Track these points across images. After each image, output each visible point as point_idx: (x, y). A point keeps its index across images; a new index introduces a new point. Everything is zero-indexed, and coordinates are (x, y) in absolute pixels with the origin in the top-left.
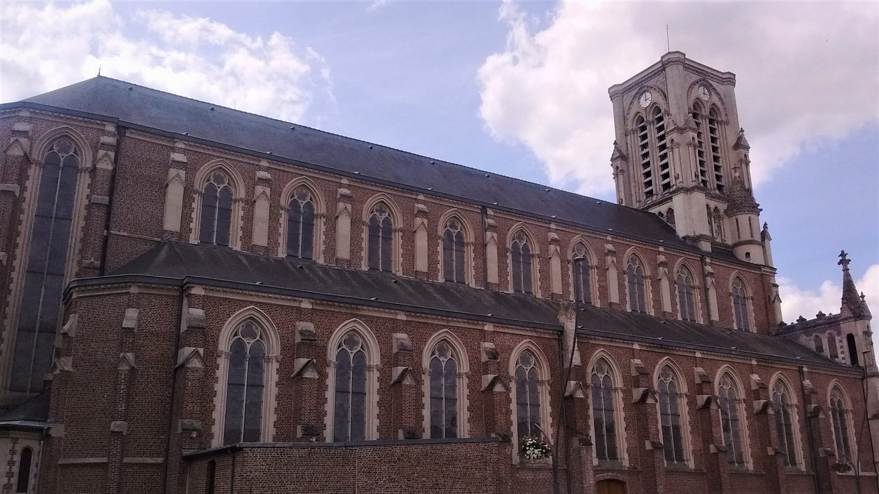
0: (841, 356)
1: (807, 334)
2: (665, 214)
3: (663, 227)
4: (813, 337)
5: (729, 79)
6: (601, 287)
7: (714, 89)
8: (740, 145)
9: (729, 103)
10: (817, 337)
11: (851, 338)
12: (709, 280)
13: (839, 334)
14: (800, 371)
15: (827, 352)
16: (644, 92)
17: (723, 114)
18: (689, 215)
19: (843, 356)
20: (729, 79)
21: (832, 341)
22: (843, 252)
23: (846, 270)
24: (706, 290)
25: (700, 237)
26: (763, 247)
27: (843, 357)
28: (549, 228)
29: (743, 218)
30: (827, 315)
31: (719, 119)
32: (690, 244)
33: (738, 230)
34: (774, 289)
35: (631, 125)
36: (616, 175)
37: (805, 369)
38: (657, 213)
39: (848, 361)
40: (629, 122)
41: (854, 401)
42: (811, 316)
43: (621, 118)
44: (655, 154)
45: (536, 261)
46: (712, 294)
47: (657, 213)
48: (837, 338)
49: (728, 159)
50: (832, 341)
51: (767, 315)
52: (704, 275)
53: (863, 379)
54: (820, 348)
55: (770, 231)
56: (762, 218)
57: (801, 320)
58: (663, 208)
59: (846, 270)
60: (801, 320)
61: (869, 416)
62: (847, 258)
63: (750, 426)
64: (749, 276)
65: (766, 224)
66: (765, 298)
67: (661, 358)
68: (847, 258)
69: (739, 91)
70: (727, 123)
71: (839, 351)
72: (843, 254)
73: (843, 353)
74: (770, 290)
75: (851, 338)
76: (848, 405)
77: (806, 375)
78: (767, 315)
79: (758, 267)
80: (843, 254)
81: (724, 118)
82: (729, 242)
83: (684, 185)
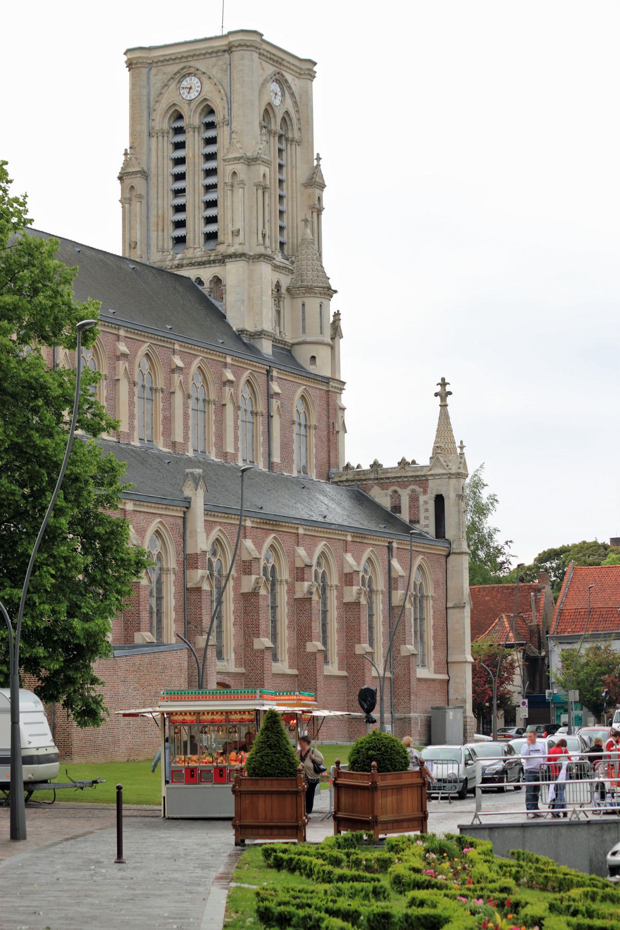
0: (423, 522)
1: (383, 487)
2: (207, 284)
3: (205, 304)
4: (390, 492)
5: (307, 69)
6: (165, 418)
7: (289, 87)
8: (315, 182)
9: (303, 105)
10: (395, 492)
11: (439, 500)
12: (275, 403)
13: (425, 492)
14: (390, 548)
15: (405, 516)
16: (189, 74)
17: (296, 127)
18: (248, 299)
19: (427, 522)
20: (307, 69)
21: (414, 499)
22: (443, 379)
23: (444, 406)
24: (270, 417)
25: (260, 334)
26: (332, 348)
27: (427, 524)
28: (118, 336)
29: (312, 303)
30: (380, 430)
31: (290, 135)
32: (245, 342)
33: (304, 320)
34: (340, 414)
35: (162, 123)
36: (126, 201)
37: (395, 545)
38: (193, 279)
39: (432, 530)
40: (157, 116)
41: (437, 584)
42: (390, 462)
43: (141, 105)
44: (195, 182)
45: (103, 383)
46: (276, 423)
47: (193, 279)
48: (422, 499)
49: (296, 209)
50: (414, 499)
51: (329, 452)
52: (270, 396)
53: (448, 556)
54: (397, 508)
55: (344, 325)
56: (335, 305)
57: (376, 465)
58: (206, 274)
59: (444, 406)
60: (376, 465)
61: (449, 605)
62: (448, 388)
63: (340, 617)
64: (316, 392)
65: (337, 314)
66: (329, 426)
67: (267, 536)
68: (448, 388)
69: (318, 87)
70: (299, 143)
71: (422, 515)
72: (443, 384)
73: (427, 518)
74: (336, 415)
75: (439, 500)
76: (430, 591)
77: (395, 551)
78: (329, 452)
79: (326, 381)
80: (443, 384)
81: (296, 135)
82: (289, 339)
83: (246, 250)
